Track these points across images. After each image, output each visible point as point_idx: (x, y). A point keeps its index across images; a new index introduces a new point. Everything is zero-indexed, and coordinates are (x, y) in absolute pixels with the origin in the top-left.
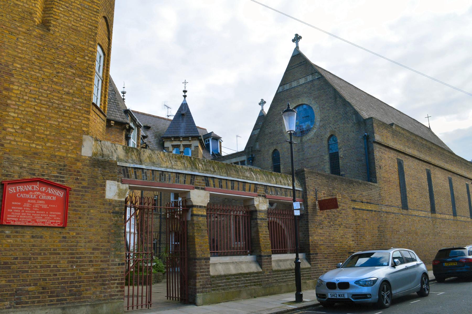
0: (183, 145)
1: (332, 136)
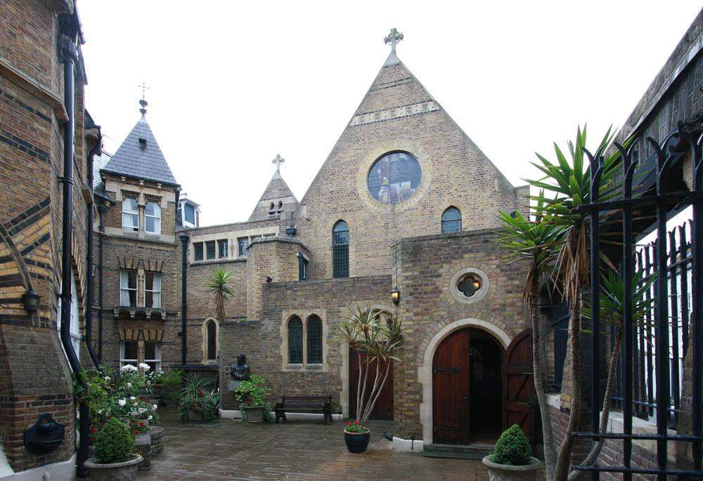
0: (145, 194)
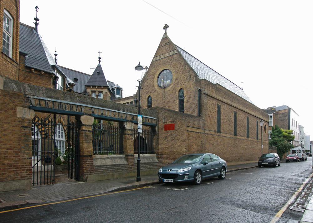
0: (98, 91)
1: (181, 89)
